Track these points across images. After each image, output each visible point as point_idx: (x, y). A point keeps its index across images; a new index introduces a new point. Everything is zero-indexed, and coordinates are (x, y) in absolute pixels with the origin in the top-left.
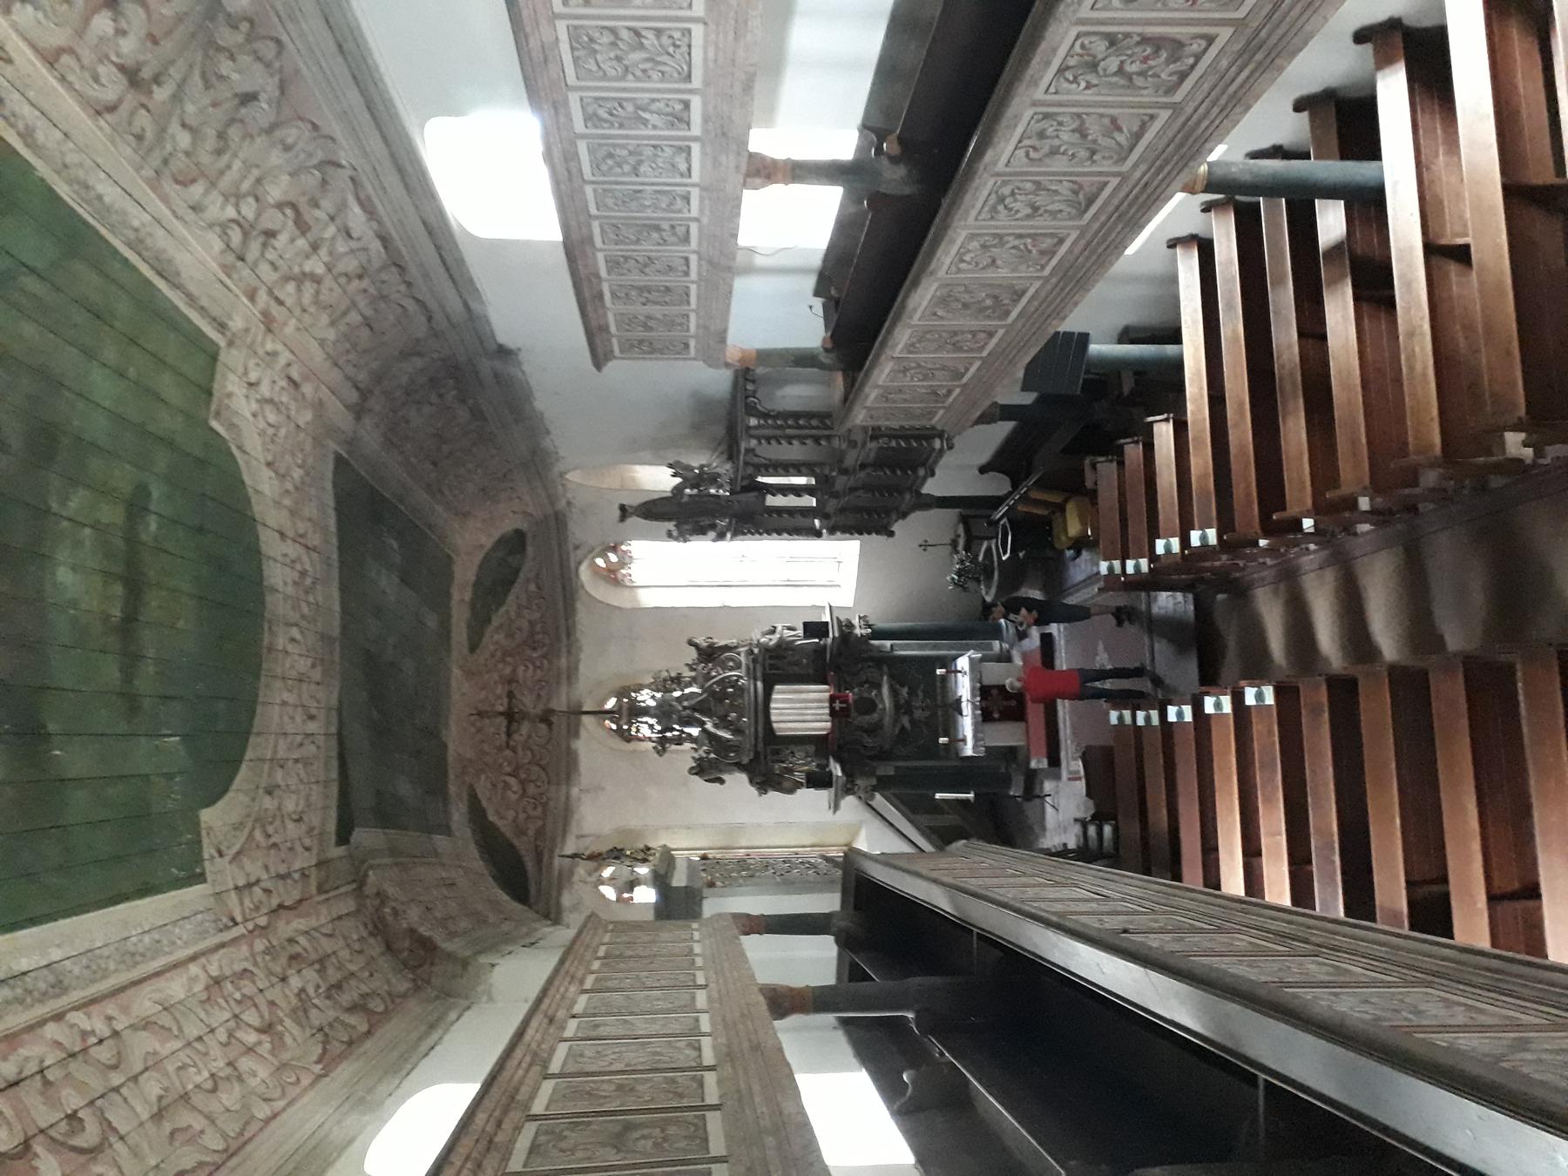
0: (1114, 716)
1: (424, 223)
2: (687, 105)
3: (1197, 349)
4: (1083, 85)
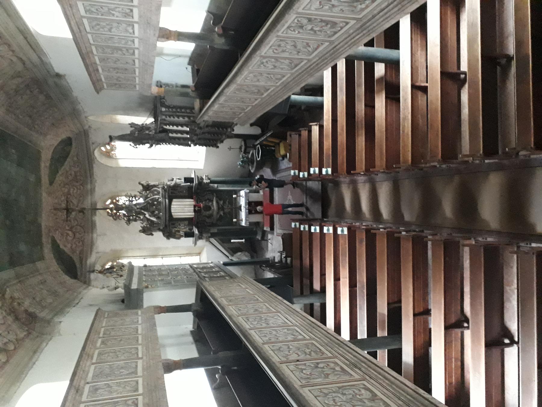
0: (293, 225)
1: (18, 28)
2: (132, 11)
3: (329, 102)
4: (297, 32)
